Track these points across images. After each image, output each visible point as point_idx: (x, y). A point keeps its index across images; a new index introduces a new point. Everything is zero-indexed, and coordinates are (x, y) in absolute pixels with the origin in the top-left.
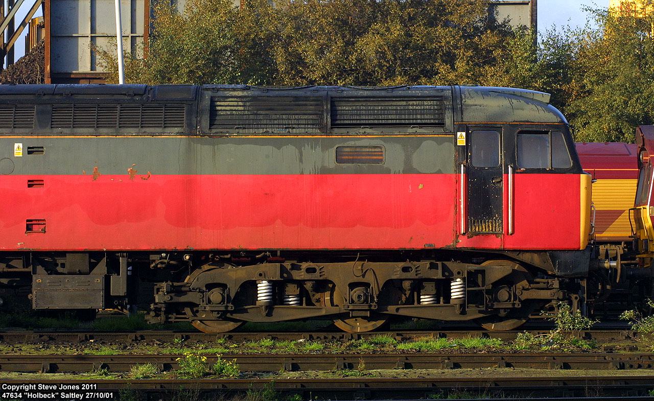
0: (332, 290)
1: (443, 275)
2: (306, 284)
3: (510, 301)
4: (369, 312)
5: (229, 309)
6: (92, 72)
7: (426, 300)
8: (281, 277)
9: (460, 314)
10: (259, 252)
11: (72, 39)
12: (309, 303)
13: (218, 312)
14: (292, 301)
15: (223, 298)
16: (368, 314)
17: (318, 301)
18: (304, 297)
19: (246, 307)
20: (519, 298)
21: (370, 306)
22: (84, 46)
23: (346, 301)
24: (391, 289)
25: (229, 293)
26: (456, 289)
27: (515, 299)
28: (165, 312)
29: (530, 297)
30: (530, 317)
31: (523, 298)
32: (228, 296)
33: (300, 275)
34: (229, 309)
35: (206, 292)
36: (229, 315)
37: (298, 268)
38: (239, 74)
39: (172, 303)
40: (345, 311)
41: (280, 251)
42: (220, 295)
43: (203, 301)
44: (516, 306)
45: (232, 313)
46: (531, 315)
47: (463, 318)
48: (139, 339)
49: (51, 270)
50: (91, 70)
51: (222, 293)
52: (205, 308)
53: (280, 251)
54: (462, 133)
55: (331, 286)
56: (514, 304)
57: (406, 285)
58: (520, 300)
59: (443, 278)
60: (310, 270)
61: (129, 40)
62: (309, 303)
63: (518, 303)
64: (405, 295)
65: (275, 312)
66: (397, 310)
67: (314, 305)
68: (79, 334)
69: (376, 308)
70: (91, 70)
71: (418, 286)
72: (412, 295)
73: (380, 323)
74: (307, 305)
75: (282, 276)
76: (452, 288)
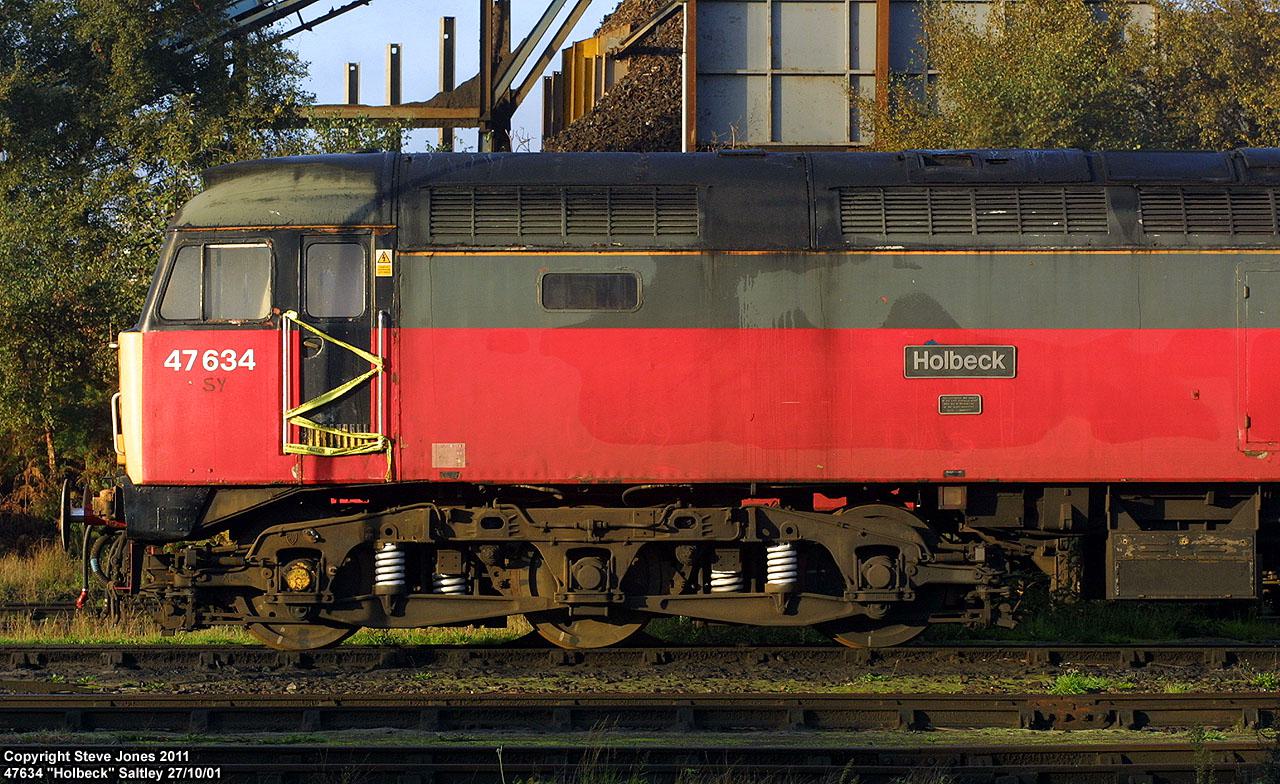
0: (535, 563)
1: (759, 534)
2: (480, 551)
3: (893, 588)
4: (606, 608)
5: (324, 600)
6: (775, 144)
7: (721, 580)
8: (431, 538)
9: (785, 613)
10: (894, 485)
11: (736, 78)
12: (487, 588)
13: (883, 604)
14: (448, 586)
15: (603, 577)
16: (605, 611)
17: (506, 585)
18: (478, 582)
19: (358, 598)
20: (910, 580)
21: (610, 596)
22: (758, 93)
23: (562, 584)
24: (655, 561)
25: (615, 571)
26: (778, 563)
27: (902, 584)
28: (196, 606)
29: (931, 580)
30: (931, 620)
31: (919, 581)
32: (613, 577)
33: (465, 532)
34: (324, 600)
35: (278, 566)
36: (323, 614)
37: (466, 518)
38: (1139, 147)
39: (211, 587)
40: (558, 606)
41: (757, 484)
42: (597, 571)
43: (272, 584)
44: (906, 598)
45: (330, 608)
46: (933, 617)
47: (789, 621)
48: (573, 661)
49: (1151, 520)
50: (851, 141)
51: (600, 567)
52: (276, 599)
53: (757, 484)
54: (386, 251)
55: (531, 554)
56: (610, 596)
57: (683, 554)
58: (913, 586)
59: (758, 540)
60: (487, 523)
61: (769, 79)
62: (487, 588)
63: (910, 591)
64: (683, 575)
65: (802, 605)
66: (664, 604)
67: (499, 594)
68: (1122, 651)
69: (622, 601)
70: (851, 141)
71: (706, 556)
72: (693, 578)
73: (630, 629)
74: (482, 592)
75: (432, 534)
76: (769, 563)
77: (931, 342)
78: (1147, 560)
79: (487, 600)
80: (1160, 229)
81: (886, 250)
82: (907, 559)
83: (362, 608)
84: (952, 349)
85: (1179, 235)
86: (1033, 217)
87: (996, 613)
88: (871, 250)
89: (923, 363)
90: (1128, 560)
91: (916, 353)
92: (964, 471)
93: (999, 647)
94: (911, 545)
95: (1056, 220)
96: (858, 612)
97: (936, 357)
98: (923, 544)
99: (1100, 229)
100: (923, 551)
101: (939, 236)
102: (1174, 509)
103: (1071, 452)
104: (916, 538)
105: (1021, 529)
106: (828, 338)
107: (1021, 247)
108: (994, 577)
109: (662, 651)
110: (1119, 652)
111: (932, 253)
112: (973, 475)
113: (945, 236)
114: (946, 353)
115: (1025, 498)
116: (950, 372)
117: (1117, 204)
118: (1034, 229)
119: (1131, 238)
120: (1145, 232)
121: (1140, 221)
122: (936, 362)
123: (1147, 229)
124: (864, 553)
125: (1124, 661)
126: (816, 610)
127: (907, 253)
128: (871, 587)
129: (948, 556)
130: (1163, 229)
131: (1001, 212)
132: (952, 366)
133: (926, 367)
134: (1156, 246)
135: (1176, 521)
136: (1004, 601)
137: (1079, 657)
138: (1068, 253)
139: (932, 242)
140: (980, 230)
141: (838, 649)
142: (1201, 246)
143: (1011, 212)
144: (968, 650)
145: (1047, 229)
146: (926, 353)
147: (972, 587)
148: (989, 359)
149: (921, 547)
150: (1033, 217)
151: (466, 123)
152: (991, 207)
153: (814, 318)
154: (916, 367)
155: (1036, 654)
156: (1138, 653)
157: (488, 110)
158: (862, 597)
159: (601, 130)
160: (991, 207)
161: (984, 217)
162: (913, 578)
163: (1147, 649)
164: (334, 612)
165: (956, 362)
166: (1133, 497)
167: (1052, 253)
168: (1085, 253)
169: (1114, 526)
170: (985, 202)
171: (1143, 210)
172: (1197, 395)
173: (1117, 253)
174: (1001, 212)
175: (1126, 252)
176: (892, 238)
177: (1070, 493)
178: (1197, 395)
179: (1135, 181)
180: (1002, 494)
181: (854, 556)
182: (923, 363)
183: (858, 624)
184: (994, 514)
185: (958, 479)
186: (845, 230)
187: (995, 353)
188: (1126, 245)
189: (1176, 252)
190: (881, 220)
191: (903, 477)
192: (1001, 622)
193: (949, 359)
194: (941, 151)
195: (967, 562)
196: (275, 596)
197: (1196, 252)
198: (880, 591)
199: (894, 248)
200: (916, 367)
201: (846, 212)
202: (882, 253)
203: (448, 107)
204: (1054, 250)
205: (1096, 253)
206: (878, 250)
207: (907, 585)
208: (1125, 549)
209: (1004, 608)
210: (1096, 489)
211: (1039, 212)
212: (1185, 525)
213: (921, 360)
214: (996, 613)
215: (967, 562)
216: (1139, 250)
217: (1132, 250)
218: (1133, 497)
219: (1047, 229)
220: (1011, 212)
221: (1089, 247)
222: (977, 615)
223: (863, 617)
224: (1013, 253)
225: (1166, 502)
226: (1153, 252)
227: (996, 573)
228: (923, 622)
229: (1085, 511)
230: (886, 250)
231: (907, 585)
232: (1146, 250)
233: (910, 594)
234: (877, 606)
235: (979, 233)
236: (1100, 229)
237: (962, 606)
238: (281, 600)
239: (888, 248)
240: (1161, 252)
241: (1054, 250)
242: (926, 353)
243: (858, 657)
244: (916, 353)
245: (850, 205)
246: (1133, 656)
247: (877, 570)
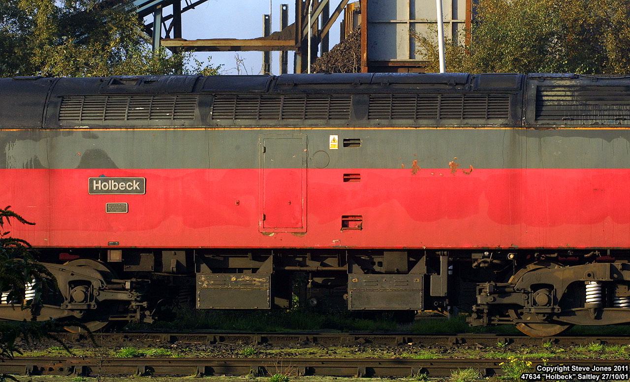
3: (550, 305)
5: (556, 311)
6: (411, 60)
13: (81, 311)
20: (96, 298)
25: (556, 295)
32: (555, 297)
34: (556, 311)
36: (555, 318)
42: (83, 293)
43: (528, 303)
44: (92, 307)
45: (558, 315)
46: (111, 317)
48: (460, 342)
49: (368, 268)
58: (97, 301)
70: (410, 58)
77: (103, 175)
78: (214, 289)
79: (49, 307)
80: (220, 117)
81: (81, 128)
82: (94, 288)
83: (576, 315)
84: (113, 179)
85: (231, 120)
86: (157, 111)
87: (143, 316)
88: (72, 129)
89: (98, 187)
90: (205, 288)
91: (95, 181)
92: (118, 242)
93: (145, 333)
94: (96, 280)
95: (168, 113)
96: (70, 315)
97: (105, 183)
98: (103, 280)
99: (190, 117)
100: (102, 283)
101: (107, 121)
102: (234, 262)
103: (174, 234)
104: (99, 276)
105: (153, 272)
106: (51, 172)
107: (149, 127)
108: (138, 297)
109: (508, 338)
110: (206, 336)
111: (103, 130)
112: (123, 244)
113: (111, 121)
114: (110, 181)
115: (154, 255)
116: (112, 191)
117: (201, 104)
118: (156, 117)
119: (204, 121)
120: (213, 119)
121: (211, 113)
122: (105, 186)
123: (214, 117)
124: (73, 284)
125: (208, 340)
126: (49, 313)
127: (91, 130)
128: (75, 302)
129: (115, 286)
130: (222, 117)
131: (141, 108)
132: (113, 188)
133: (100, 189)
134: (217, 126)
135: (236, 269)
136: (146, 309)
137: (187, 338)
138: (173, 129)
139: (104, 124)
140: (129, 118)
141: (64, 333)
142: (241, 126)
143: (146, 108)
144: (130, 334)
145: (163, 117)
146: (100, 181)
147: (129, 302)
148: (132, 184)
149: (100, 280)
150: (157, 111)
151: (291, 48)
152: (135, 106)
153: (44, 163)
154: (95, 189)
155: (163, 337)
156: (216, 337)
157: (300, 41)
158: (70, 307)
159: (342, 52)
160: (135, 106)
161: (133, 111)
162: (97, 297)
163: (221, 335)
164: (560, 317)
165: (115, 186)
166: (212, 256)
167: (164, 129)
168: (181, 129)
169: (199, 271)
170: (135, 103)
171: (214, 107)
172: (238, 203)
173: (197, 129)
174: (141, 108)
175: (202, 129)
176: (84, 122)
177: (175, 254)
178: (238, 203)
179: (213, 92)
180: (144, 254)
181: (68, 286)
182: (98, 187)
183: (70, 321)
184: (139, 265)
185: (115, 246)
186: (60, 118)
187: (134, 181)
188: (203, 125)
189: (228, 129)
190: (79, 113)
191: (88, 245)
192: (146, 320)
193: (112, 185)
194: (125, 77)
195: (124, 289)
196: (530, 309)
197: (238, 129)
198: (80, 304)
199: (84, 127)
200: (95, 189)
201: (63, 109)
202: (78, 130)
203: (279, 40)
204: (166, 128)
205: (187, 129)
206: (76, 128)
207: (94, 301)
208: (203, 282)
209: (147, 313)
210: (189, 252)
211: (161, 108)
212: (241, 270)
213: (97, 185)
214: (143, 316)
215: (124, 289)
216: (209, 128)
217: (205, 128)
218: (212, 256)
219: (163, 117)
220: (146, 108)
221: (183, 126)
222: (134, 317)
223: (73, 317)
224: (144, 130)
225: (230, 258)
226: (216, 129)
227: (139, 295)
228: (107, 320)
229: (184, 263)
230: (81, 128)
231: (94, 301)
232: (212, 128)
233: (94, 305)
234: (78, 311)
235: (128, 119)
236: (190, 117)
237: (127, 311)
238: (533, 311)
239: (81, 127)
240: (220, 129)
241: (166, 128)
242: (100, 181)
243: (73, 338)
244: (95, 181)
245: (66, 105)
246: (213, 339)
247: (78, 293)
